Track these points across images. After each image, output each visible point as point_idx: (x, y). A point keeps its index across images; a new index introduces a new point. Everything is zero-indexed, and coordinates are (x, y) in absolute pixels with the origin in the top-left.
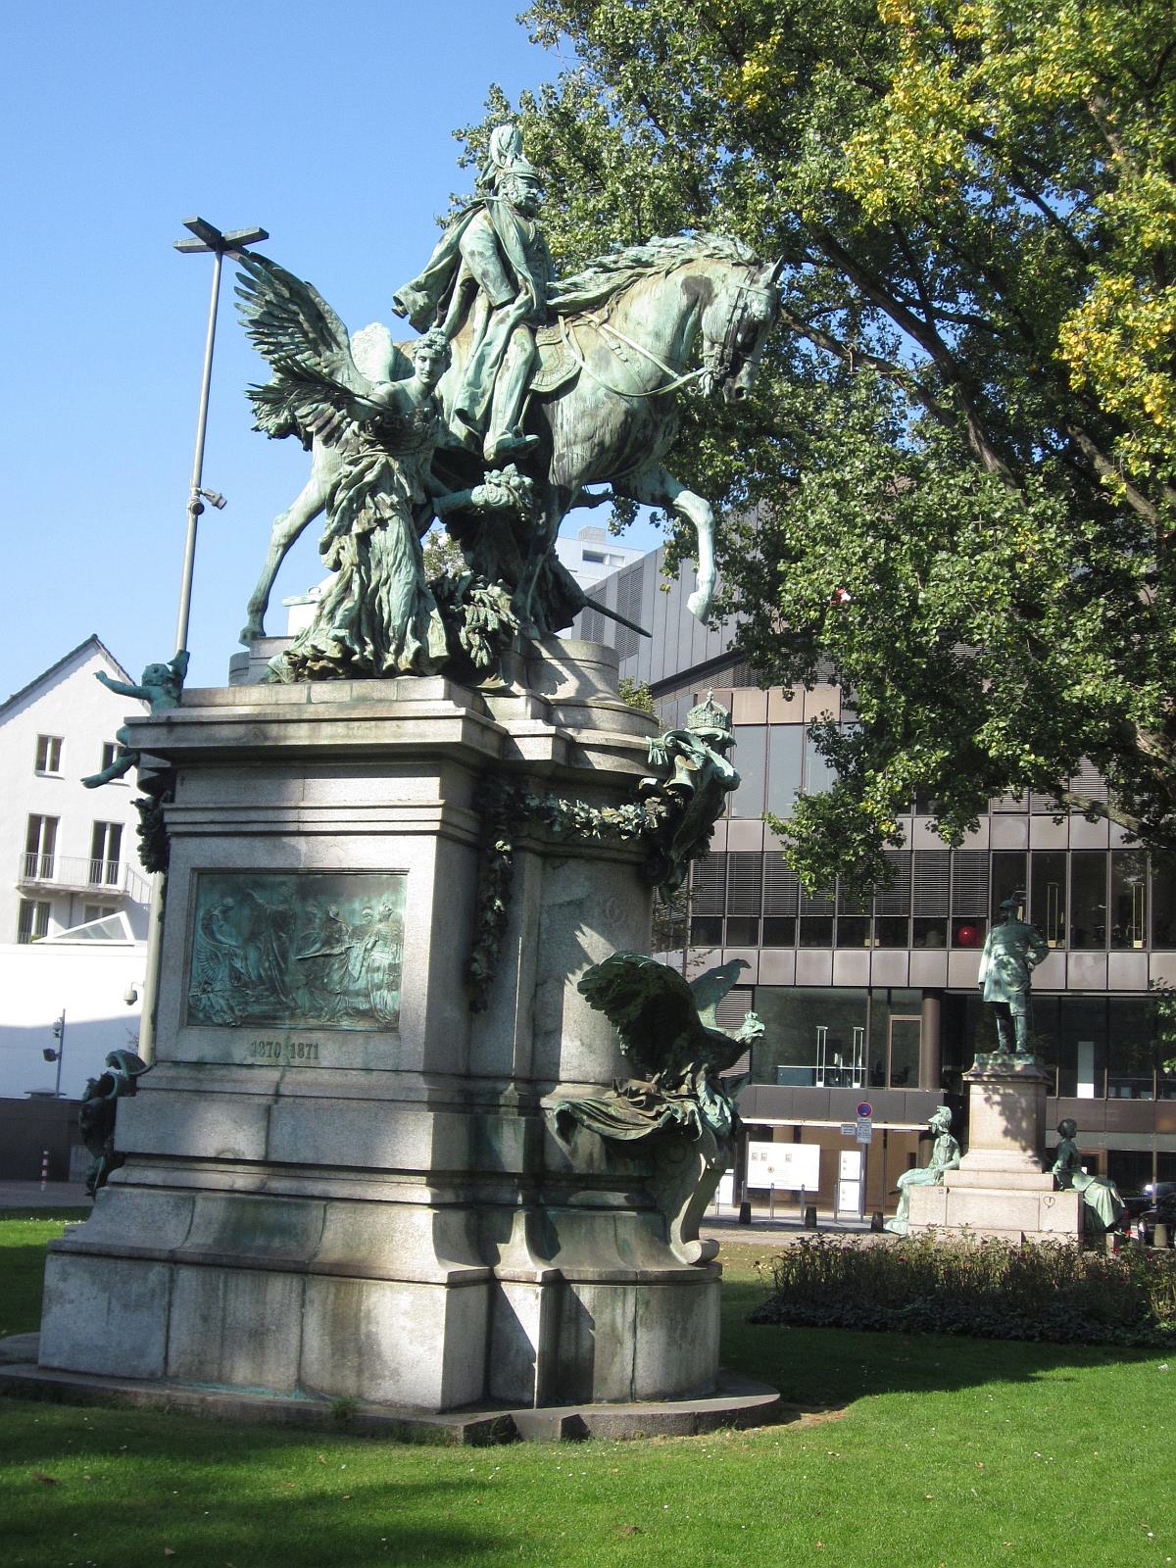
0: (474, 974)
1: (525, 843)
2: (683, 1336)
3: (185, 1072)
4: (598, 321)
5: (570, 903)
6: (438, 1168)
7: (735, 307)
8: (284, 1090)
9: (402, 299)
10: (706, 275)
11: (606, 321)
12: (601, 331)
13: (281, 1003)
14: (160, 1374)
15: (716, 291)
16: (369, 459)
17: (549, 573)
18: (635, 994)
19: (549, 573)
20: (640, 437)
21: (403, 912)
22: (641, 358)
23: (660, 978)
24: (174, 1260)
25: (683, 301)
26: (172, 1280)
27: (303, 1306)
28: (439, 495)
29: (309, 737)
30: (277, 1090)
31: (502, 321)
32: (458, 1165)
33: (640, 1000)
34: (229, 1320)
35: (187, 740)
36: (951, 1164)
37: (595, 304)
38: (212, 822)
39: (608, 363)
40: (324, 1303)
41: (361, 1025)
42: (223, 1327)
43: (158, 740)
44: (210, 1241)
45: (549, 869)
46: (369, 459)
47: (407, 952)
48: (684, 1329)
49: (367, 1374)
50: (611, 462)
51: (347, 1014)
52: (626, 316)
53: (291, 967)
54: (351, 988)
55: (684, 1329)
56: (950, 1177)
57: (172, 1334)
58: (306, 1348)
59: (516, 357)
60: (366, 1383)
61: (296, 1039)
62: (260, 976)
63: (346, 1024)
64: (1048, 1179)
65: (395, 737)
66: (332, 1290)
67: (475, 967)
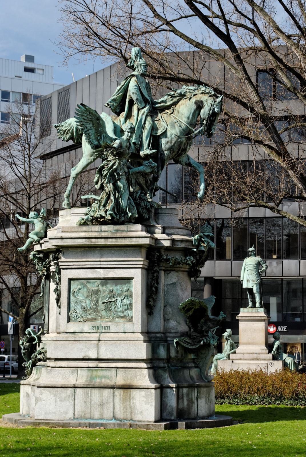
0: (150, 305)
1: (161, 268)
2: (209, 401)
3: (70, 335)
4: (170, 113)
5: (172, 284)
6: (148, 358)
7: (210, 110)
8: (101, 339)
9: (110, 104)
10: (201, 100)
11: (172, 113)
12: (171, 116)
13: (97, 315)
14: (72, 418)
15: (204, 105)
16: (114, 161)
17: (149, 181)
18: (193, 308)
19: (149, 181)
20: (184, 147)
21: (133, 289)
22: (184, 125)
23: (199, 304)
24: (75, 387)
25: (194, 107)
26: (75, 392)
27: (114, 396)
28: (131, 168)
29: (104, 242)
30: (99, 339)
31: (143, 114)
32: (150, 357)
33: (193, 310)
34: (92, 402)
35: (67, 243)
36: (232, 351)
37: (168, 107)
38: (74, 265)
39: (175, 127)
40: (120, 395)
41: (122, 320)
42: (91, 404)
43: (58, 242)
44: (84, 381)
45: (166, 274)
46: (114, 161)
47: (134, 300)
48: (209, 399)
49: (133, 413)
50: (176, 155)
51: (117, 317)
52: (178, 111)
53: (99, 304)
54: (118, 310)
55: (209, 399)
56: (232, 356)
57: (75, 407)
58: (116, 408)
59: (148, 125)
60: (133, 416)
61: (103, 325)
62: (90, 308)
63: (117, 320)
64: (270, 356)
65: (130, 242)
66: (122, 392)
67: (150, 303)
